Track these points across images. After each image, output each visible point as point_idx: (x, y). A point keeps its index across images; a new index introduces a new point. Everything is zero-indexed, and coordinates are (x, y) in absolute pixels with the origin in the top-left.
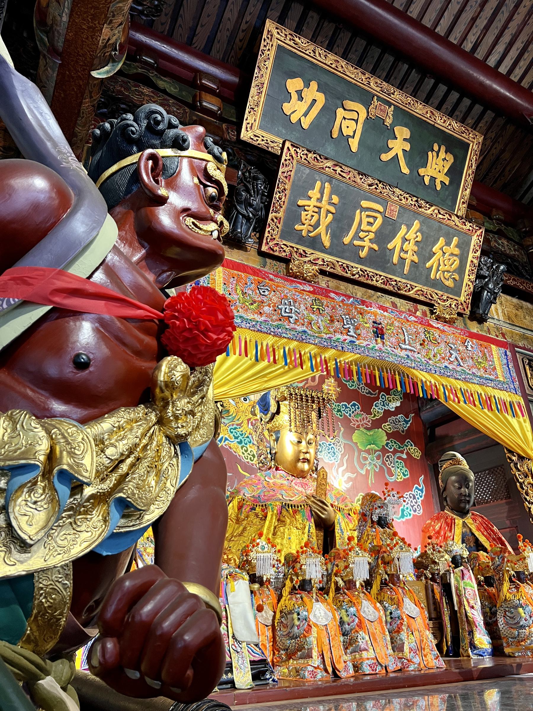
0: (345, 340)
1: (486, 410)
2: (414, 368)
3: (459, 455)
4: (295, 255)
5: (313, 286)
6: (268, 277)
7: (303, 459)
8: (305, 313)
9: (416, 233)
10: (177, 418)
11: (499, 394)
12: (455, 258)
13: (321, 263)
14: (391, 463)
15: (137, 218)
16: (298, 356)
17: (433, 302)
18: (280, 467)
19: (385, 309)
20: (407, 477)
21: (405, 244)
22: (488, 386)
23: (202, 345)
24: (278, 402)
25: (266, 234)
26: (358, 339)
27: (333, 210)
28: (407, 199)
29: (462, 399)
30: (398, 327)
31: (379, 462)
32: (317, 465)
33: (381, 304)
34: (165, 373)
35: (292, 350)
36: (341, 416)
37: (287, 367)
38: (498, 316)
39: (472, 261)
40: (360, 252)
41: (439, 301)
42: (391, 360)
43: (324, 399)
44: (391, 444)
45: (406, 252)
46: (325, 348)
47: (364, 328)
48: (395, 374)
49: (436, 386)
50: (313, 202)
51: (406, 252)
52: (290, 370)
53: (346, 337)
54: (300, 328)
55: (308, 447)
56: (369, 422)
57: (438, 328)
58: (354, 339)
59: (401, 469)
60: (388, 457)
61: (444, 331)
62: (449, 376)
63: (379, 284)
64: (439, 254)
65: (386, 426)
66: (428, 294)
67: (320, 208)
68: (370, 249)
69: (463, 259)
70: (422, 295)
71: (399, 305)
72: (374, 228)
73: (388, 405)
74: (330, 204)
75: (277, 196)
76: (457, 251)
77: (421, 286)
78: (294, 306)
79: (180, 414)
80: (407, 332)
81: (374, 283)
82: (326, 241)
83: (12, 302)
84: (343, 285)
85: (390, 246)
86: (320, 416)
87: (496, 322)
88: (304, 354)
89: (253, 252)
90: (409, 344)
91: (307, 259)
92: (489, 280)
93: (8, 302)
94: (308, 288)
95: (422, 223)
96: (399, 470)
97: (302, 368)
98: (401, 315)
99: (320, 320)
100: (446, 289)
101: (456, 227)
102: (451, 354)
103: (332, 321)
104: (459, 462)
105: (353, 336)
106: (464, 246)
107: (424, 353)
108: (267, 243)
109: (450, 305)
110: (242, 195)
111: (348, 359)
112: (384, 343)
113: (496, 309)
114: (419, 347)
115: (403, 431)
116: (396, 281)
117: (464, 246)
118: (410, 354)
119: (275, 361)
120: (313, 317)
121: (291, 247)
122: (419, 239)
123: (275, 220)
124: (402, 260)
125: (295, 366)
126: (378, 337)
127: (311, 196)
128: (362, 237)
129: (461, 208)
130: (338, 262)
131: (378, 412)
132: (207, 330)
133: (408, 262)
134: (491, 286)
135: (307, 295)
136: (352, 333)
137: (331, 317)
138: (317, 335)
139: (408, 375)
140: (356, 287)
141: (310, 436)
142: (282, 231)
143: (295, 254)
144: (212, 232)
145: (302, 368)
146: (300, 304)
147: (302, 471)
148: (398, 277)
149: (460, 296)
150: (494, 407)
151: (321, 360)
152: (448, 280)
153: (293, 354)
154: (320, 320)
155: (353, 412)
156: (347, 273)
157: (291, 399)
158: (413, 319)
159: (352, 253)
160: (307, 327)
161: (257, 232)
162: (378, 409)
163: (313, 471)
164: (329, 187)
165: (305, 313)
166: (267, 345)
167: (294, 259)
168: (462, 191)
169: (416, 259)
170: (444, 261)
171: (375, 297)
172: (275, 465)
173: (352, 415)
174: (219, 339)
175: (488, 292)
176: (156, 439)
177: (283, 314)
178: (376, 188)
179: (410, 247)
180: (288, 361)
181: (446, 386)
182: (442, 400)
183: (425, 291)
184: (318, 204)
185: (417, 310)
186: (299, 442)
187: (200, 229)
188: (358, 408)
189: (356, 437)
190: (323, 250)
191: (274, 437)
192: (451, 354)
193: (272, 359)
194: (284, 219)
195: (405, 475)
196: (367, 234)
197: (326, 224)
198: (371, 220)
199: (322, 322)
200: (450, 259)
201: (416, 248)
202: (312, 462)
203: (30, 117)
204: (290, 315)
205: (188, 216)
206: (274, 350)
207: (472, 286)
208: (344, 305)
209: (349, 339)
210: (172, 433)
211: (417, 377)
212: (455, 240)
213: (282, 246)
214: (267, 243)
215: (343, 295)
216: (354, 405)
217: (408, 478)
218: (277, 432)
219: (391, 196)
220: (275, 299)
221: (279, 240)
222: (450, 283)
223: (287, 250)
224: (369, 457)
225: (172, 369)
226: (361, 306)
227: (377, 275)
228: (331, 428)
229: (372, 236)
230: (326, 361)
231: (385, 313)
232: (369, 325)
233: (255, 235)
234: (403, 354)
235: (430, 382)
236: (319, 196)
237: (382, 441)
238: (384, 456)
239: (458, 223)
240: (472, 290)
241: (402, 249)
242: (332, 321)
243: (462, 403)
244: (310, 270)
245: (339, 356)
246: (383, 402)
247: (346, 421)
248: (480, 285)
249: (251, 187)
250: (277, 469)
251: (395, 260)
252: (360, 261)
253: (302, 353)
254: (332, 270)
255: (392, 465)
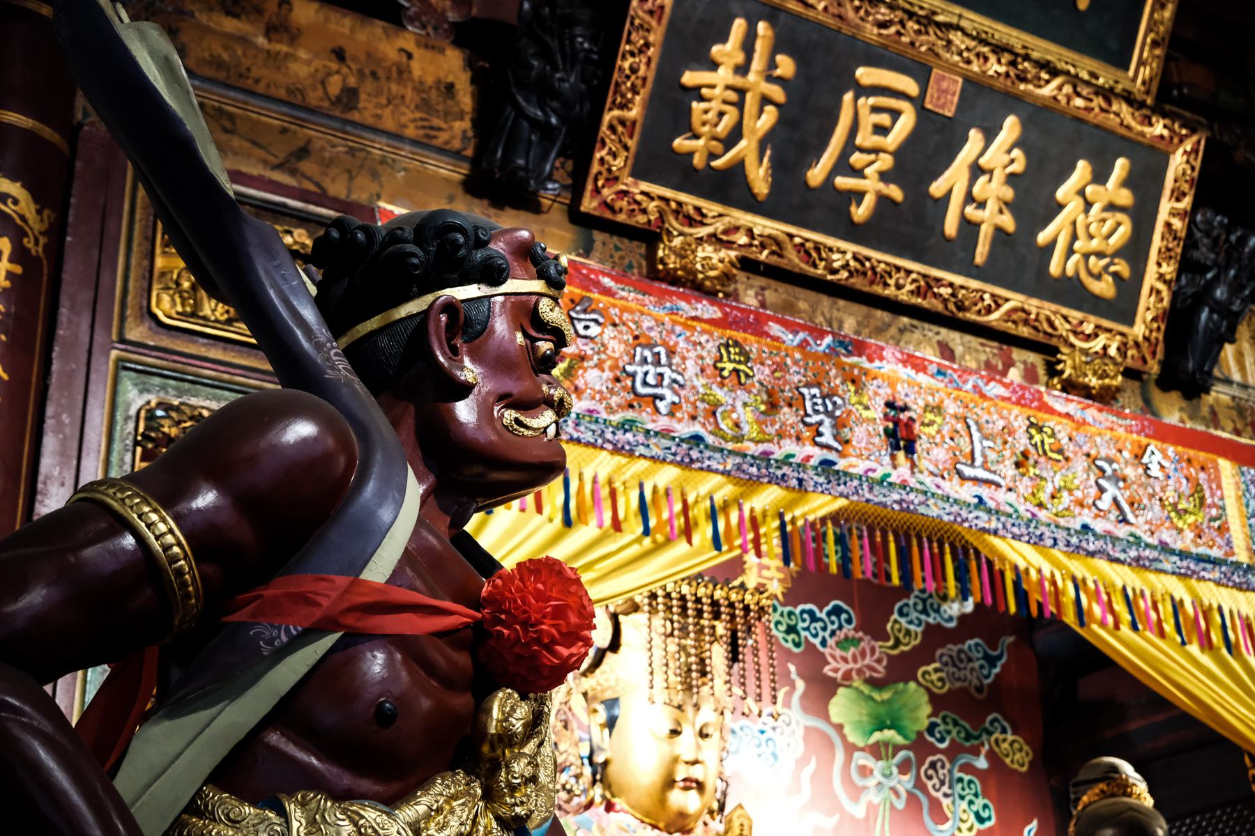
0: (808, 458)
1: (1194, 648)
2: (995, 533)
3: (1127, 768)
4: (674, 223)
5: (721, 306)
6: (597, 284)
7: (685, 780)
8: (700, 382)
9: (1009, 151)
10: (513, 789)
11: (1235, 600)
12: (1121, 217)
13: (743, 240)
14: (942, 783)
15: (419, 419)
16: (678, 507)
17: (1054, 342)
18: (619, 802)
19: (919, 365)
20: (988, 824)
21: (980, 178)
22: (1203, 579)
23: (545, 666)
24: (615, 618)
25: (595, 168)
26: (842, 454)
27: (777, 93)
28: (986, 59)
29: (1126, 617)
30: (956, 417)
31: (907, 781)
32: (724, 794)
33: (910, 349)
34: (498, 721)
35: (661, 491)
36: (797, 645)
37: (647, 542)
38: (1244, 375)
39: (1168, 225)
40: (853, 209)
41: (1072, 339)
42: (934, 511)
43: (747, 609)
44: (942, 727)
45: (982, 205)
46: (753, 484)
47: (861, 421)
48: (942, 553)
49: (1054, 583)
50: (724, 75)
51: (982, 205)
52: (657, 548)
53: (810, 449)
54: (684, 429)
55: (699, 747)
56: (879, 661)
57: (1068, 416)
58: (832, 456)
59: (971, 802)
60: (933, 765)
61: (1084, 423)
62: (1092, 554)
63: (903, 296)
64: (1073, 207)
65: (931, 671)
66: (1042, 317)
67: (742, 92)
68: (882, 199)
69: (1142, 216)
70: (1026, 322)
71: (959, 350)
72: (893, 140)
73: (937, 611)
74: (770, 79)
75: (626, 65)
76: (1125, 197)
77: (1021, 297)
78: (670, 365)
79: (519, 784)
80: (980, 429)
81: (890, 292)
82: (759, 178)
83: (294, 633)
84: (804, 300)
85: (937, 188)
86: (734, 655)
87: (1235, 391)
88: (696, 502)
89: (557, 214)
90: (984, 466)
91: (703, 232)
92: (1216, 278)
93: (287, 631)
94: (707, 310)
95: (1025, 124)
96: (964, 805)
97: (690, 542)
98: (965, 382)
99: (739, 404)
100: (1093, 304)
101: (1123, 131)
102: (1102, 490)
103: (773, 406)
104: (1124, 788)
105: (829, 447)
106: (1146, 184)
107: (1024, 486)
108: (597, 191)
109: (1105, 348)
110: (532, 67)
111: (814, 511)
112: (913, 465)
113: (1240, 356)
114: (1010, 471)
115: (979, 689)
116: (951, 285)
117: (1146, 184)
118: (985, 492)
119: (617, 525)
120: (720, 394)
121: (661, 198)
122: (1018, 167)
123: (620, 129)
124: (969, 227)
125: (669, 540)
126: (898, 448)
127: (720, 59)
128: (858, 166)
129: (1142, 70)
130: (791, 236)
131: (908, 633)
132: (554, 642)
133: (985, 232)
134: (1219, 293)
135: (703, 332)
136: (827, 438)
137: (770, 393)
138: (730, 446)
139: (977, 553)
140: (841, 303)
141: (707, 715)
142: (638, 156)
143: (672, 219)
144: (546, 428)
145: (690, 542)
146: (684, 359)
147: (682, 815)
148: (959, 273)
149: (1131, 323)
150: (1216, 637)
151: (741, 518)
152: (1098, 277)
153: (663, 502)
154: (739, 404)
155: (833, 633)
156: (815, 266)
157: (653, 611)
158: (1001, 391)
159: (829, 209)
160: (704, 425)
161: (567, 157)
162: (906, 625)
163: (711, 812)
164: (770, 33)
165: (700, 382)
166: (595, 481)
167: (669, 233)
168: (1152, 11)
169: (1008, 222)
170: (1088, 226)
171: (893, 331)
172: (604, 797)
173: (831, 642)
174: (572, 655)
175: (1211, 311)
176: (482, 822)
177: (641, 389)
178: (899, 34)
179: (994, 189)
180: (652, 523)
181: (1084, 580)
182: (1070, 618)
183: (1034, 311)
184: (738, 81)
185: (1009, 364)
186: (675, 733)
187: (527, 427)
188: (849, 621)
189: (842, 706)
190: (751, 204)
191: (602, 716)
192: (1102, 490)
193: (607, 516)
194: (644, 126)
195: (981, 820)
196: (873, 157)
197: (760, 134)
198: (885, 119)
199: (742, 409)
200: (1104, 221)
201: (1009, 193)
202: (709, 787)
203: (306, 344)
204: (658, 391)
205: (507, 407)
206: (613, 494)
207: (1166, 294)
208: (806, 356)
209: (818, 454)
210: (503, 811)
211: (1003, 559)
212: (1121, 166)
213: (639, 197)
214: (597, 191)
215: (804, 328)
216: (837, 611)
217: (990, 829)
218: (611, 703)
219: (941, 52)
220: (616, 348)
221: (630, 180)
222: (1104, 288)
223: (652, 206)
224: (877, 766)
225: (507, 710)
226: (854, 359)
227: (898, 269)
228: (766, 684)
229: (885, 162)
230: (753, 520)
231: (922, 378)
232: (877, 412)
233: (563, 166)
234: (967, 492)
235: (1039, 571)
236: (740, 58)
237: (916, 720)
238: (920, 763)
239: (1129, 120)
240: (1166, 303)
241: (969, 198)
242: (773, 406)
243: (1125, 629)
244: (711, 259)
245: (791, 505)
246: (924, 601)
247: (812, 662)
248: (1190, 291)
249: (554, 44)
250: (609, 807)
251: (951, 226)
252: (852, 232)
253: (691, 499)
254: (774, 260)
255: (945, 789)
